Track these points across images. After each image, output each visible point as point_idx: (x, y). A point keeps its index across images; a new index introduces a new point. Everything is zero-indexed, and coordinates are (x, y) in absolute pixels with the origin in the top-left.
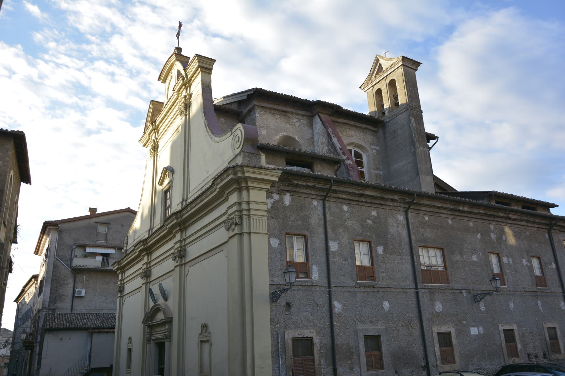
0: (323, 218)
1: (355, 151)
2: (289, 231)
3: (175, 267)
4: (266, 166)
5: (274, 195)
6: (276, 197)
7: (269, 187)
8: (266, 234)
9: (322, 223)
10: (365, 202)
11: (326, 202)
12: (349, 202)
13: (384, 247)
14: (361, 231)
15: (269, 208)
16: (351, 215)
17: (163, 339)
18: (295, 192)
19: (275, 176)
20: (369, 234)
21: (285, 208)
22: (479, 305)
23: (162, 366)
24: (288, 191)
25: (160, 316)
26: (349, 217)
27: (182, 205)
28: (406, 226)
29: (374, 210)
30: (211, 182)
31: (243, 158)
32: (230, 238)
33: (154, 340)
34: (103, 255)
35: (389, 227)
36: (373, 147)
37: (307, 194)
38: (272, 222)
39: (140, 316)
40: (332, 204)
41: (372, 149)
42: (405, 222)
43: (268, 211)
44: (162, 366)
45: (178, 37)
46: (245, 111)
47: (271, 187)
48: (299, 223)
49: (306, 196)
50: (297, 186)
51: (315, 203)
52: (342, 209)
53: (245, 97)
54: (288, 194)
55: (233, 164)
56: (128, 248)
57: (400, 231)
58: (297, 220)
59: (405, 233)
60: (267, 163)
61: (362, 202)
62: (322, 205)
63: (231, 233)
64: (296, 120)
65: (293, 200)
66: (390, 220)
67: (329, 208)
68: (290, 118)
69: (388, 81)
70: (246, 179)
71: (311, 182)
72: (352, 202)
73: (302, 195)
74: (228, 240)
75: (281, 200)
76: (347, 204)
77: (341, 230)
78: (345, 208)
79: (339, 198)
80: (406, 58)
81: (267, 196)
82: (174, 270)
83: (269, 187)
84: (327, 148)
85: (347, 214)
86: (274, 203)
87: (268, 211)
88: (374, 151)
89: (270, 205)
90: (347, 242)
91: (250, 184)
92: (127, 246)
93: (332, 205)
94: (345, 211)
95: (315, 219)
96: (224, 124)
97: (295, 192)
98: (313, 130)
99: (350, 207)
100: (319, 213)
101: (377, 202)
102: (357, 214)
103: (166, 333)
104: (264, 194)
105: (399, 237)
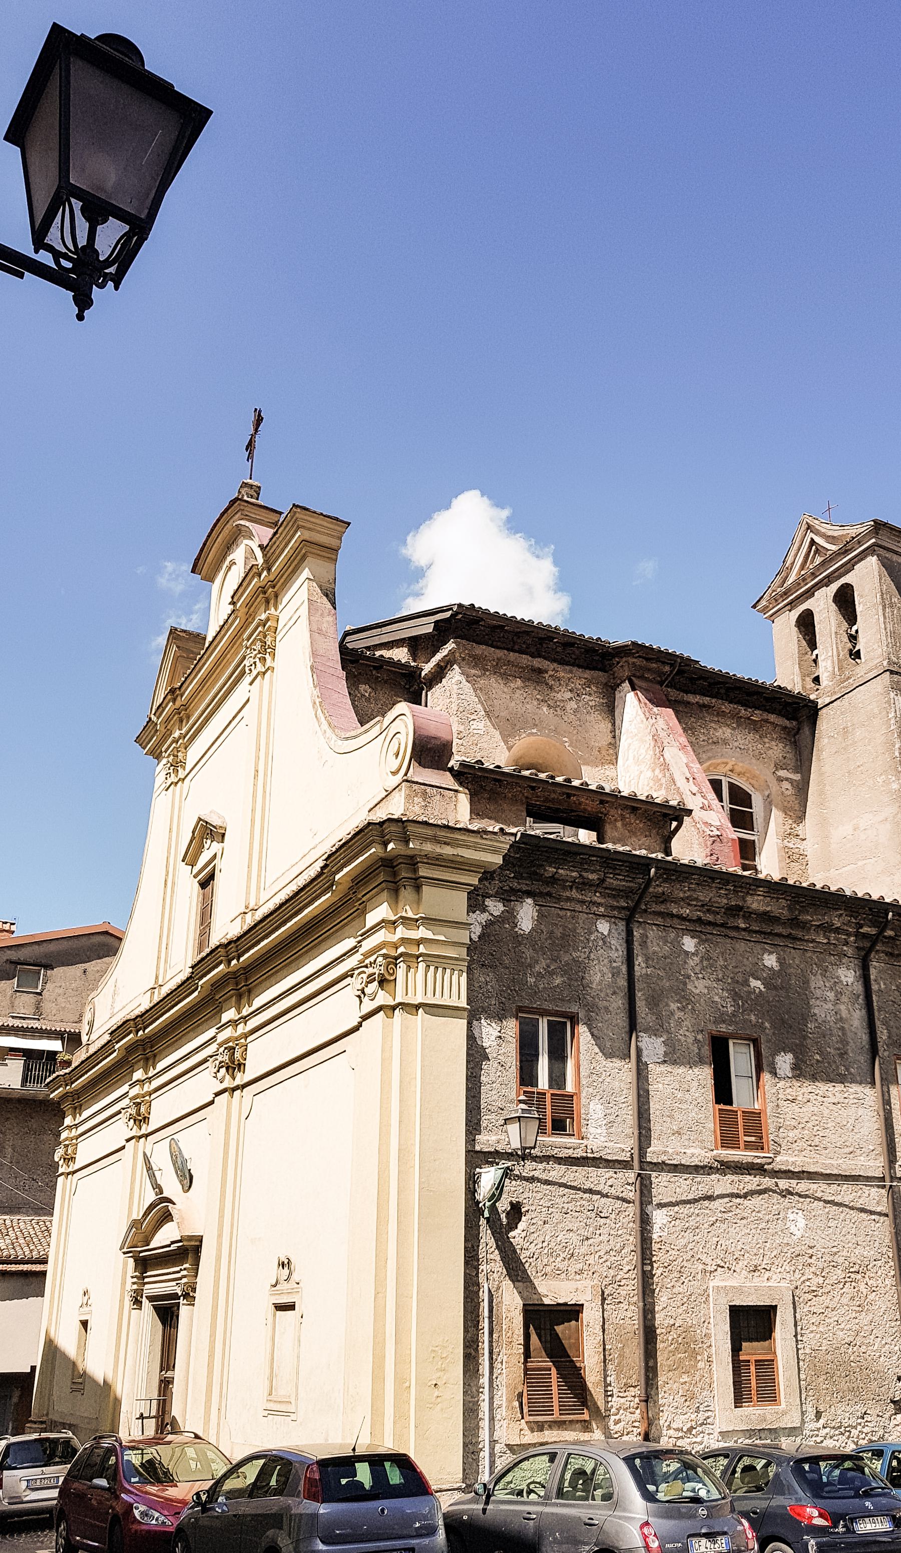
0: (624, 969)
1: (732, 786)
2: (526, 1003)
3: (217, 1094)
4: (474, 827)
5: (488, 902)
6: (496, 907)
7: (476, 882)
8: (464, 1009)
9: (623, 982)
10: (744, 930)
11: (635, 927)
12: (697, 927)
13: (796, 1057)
14: (730, 1010)
15: (475, 937)
16: (705, 963)
17: (175, 1296)
18: (549, 894)
19: (495, 851)
20: (753, 1018)
21: (518, 939)
22: (701, 1061)
23: (169, 1374)
24: (529, 894)
25: (166, 1236)
26: (697, 969)
27: (243, 921)
28: (861, 1000)
29: (771, 953)
30: (321, 863)
31: (408, 797)
32: (365, 1018)
33: (151, 1299)
34: (28, 1054)
35: (812, 1002)
36: (782, 773)
37: (583, 902)
38: (481, 977)
39: (117, 1230)
40: (653, 933)
41: (780, 780)
42: (859, 988)
43: (472, 948)
44: (169, 1374)
45: (250, 457)
46: (427, 668)
47: (480, 880)
48: (558, 981)
49: (578, 907)
50: (554, 880)
51: (603, 927)
52: (680, 945)
53: (429, 629)
54: (530, 901)
55: (380, 815)
56: (93, 1037)
57: (844, 1014)
58: (552, 973)
59: (856, 1018)
60: (475, 813)
61: (737, 928)
62: (624, 934)
63: (368, 1006)
64: (569, 695)
65: (541, 916)
66: (816, 982)
67: (644, 944)
68: (551, 688)
69: (835, 587)
70: (412, 861)
71: (593, 872)
72: (709, 929)
73: (567, 905)
74: (360, 1025)
75: (510, 917)
76: (693, 934)
77: (674, 1006)
78: (689, 944)
79: (672, 916)
80: (885, 525)
81: (469, 906)
82: (212, 1102)
83: (476, 882)
84: (649, 774)
85: (693, 962)
86: (489, 924)
87: (472, 948)
88: (786, 785)
89: (478, 930)
90: (690, 1040)
91: (423, 872)
92: (89, 1033)
93: (653, 939)
94: (687, 953)
95: (602, 970)
96: (368, 700)
97: (549, 894)
98: (614, 724)
99: (701, 942)
100: (614, 955)
101: (779, 929)
102: (721, 962)
103: (184, 1280)
104: (461, 899)
105: (842, 1029)
